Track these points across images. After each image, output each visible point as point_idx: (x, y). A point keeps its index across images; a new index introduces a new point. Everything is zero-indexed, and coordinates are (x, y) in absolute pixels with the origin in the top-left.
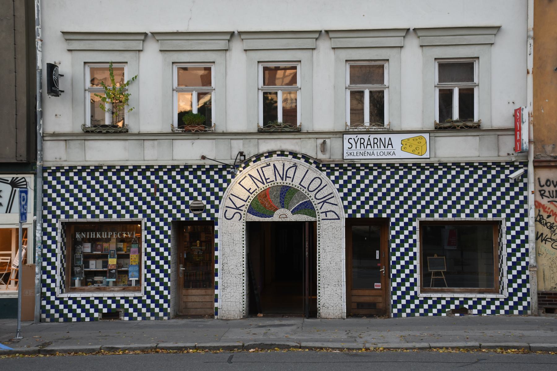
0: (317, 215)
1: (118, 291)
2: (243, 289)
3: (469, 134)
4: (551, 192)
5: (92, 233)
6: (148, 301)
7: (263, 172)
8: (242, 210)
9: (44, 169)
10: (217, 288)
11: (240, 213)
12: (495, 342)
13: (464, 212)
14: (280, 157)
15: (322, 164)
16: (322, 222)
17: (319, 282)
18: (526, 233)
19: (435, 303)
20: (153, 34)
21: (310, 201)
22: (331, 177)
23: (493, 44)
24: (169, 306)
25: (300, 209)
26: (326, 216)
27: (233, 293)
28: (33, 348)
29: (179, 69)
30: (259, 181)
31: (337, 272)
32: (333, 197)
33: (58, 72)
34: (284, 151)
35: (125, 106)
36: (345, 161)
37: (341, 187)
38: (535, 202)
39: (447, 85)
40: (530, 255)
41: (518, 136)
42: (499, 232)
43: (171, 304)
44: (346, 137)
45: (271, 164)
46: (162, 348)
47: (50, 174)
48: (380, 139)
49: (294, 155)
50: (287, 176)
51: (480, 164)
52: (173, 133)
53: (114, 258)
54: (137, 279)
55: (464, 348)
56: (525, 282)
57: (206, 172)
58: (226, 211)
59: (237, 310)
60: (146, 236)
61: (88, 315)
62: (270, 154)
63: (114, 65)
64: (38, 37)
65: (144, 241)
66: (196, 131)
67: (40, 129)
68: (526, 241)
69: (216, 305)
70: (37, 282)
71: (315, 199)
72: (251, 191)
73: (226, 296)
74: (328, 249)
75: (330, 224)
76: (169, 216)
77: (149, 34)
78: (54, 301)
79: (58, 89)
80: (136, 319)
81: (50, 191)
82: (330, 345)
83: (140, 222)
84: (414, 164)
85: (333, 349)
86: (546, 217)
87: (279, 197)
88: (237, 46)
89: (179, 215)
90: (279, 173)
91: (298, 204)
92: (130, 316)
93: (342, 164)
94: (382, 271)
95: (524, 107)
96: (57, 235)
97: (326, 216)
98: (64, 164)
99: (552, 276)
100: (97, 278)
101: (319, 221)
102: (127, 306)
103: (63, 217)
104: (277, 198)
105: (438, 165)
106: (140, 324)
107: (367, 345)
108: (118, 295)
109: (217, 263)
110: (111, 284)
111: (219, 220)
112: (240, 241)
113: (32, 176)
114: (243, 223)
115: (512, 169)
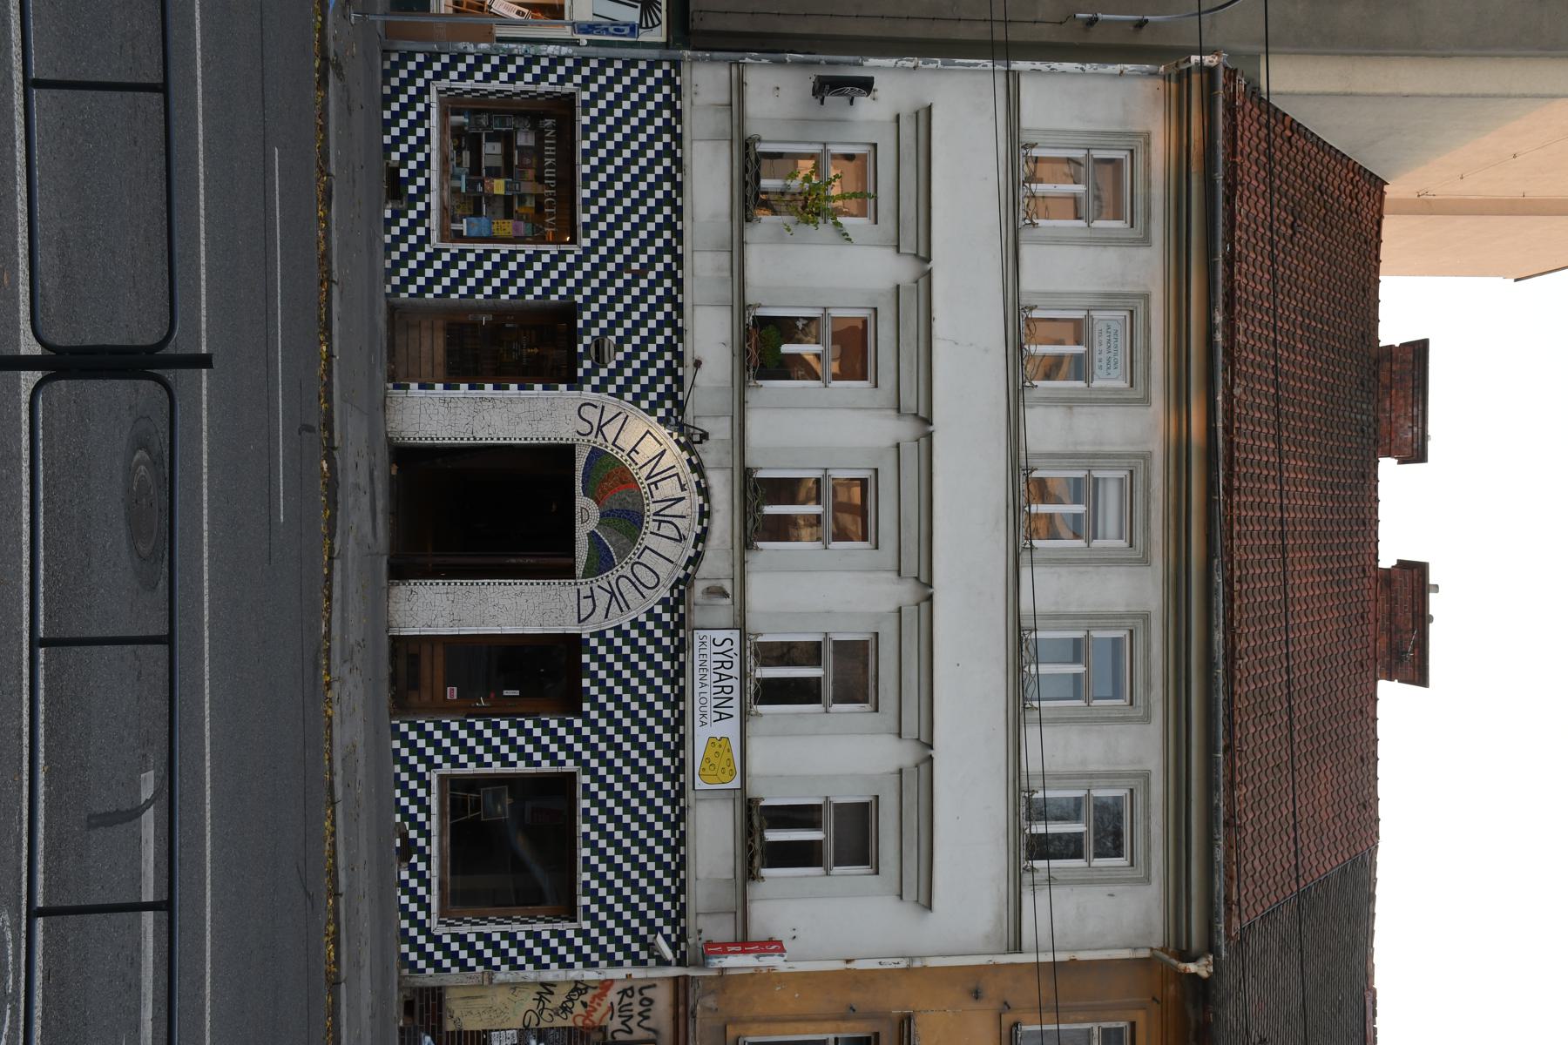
1: (441, 198)
3: (739, 861)
4: (629, 1008)
6: (421, 256)
7: (670, 477)
8: (596, 437)
9: (676, 64)
10: (446, 388)
11: (591, 432)
12: (348, 920)
18: (554, 966)
19: (420, 802)
20: (929, 274)
21: (615, 566)
23: (901, 898)
24: (411, 295)
27: (436, 418)
28: (331, 46)
29: (865, 321)
30: (653, 469)
32: (622, 611)
34: (708, 518)
35: (795, 218)
36: (690, 633)
38: (612, 981)
39: (829, 819)
40: (513, 972)
41: (733, 948)
43: (415, 299)
44: (735, 635)
46: (329, 293)
47: (667, 73)
48: (731, 698)
49: (702, 537)
51: (683, 882)
52: (744, 307)
53: (506, 189)
54: (465, 234)
55: (335, 865)
56: (462, 964)
57: (669, 369)
58: (596, 407)
59: (405, 426)
60: (547, 252)
61: (397, 141)
62: (704, 492)
63: (872, 200)
64: (920, 62)
66: (748, 351)
67: (752, 58)
68: (538, 964)
69: (414, 386)
70: (461, 45)
74: (521, 600)
76: (585, 298)
77: (929, 267)
78: (422, 76)
80: (388, 232)
81: (634, 73)
82: (336, 615)
83: (573, 241)
84: (682, 761)
85: (329, 622)
86: (584, 1000)
88: (905, 430)
89: (587, 315)
92: (394, 221)
94: (480, 702)
95: (785, 958)
96: (551, 84)
98: (686, 100)
99: (474, 1012)
100: (466, 155)
101: (576, 584)
102: (412, 214)
103: (586, 96)
105: (682, 805)
106: (378, 240)
107: (336, 685)
108: (433, 198)
109: (495, 388)
110: (456, 183)
113: (663, 39)
115: (673, 939)
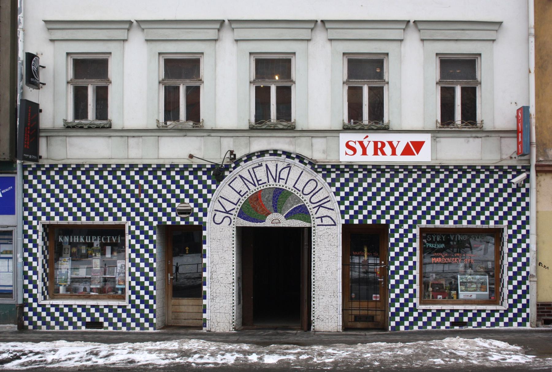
0: (312, 221)
2: (233, 300)
5: (75, 237)
6: (133, 311)
7: (254, 173)
8: (232, 214)
11: (229, 218)
13: (466, 219)
14: (273, 157)
15: (318, 165)
16: (317, 227)
17: (314, 293)
19: (434, 315)
21: (304, 205)
22: (327, 179)
25: (294, 214)
26: (322, 222)
31: (333, 282)
32: (329, 201)
33: (39, 63)
37: (338, 190)
42: (501, 241)
45: (263, 164)
47: (30, 173)
49: (288, 155)
50: (281, 177)
51: (483, 167)
58: (215, 215)
60: (130, 241)
62: (262, 153)
65: (128, 246)
69: (205, 316)
71: (310, 203)
72: (242, 194)
73: (215, 306)
74: (323, 258)
75: (326, 231)
79: (39, 80)
87: (272, 200)
88: (227, 37)
89: (164, 219)
90: (271, 174)
91: (292, 208)
93: (339, 165)
97: (322, 222)
101: (314, 227)
103: (44, 218)
104: (270, 201)
111: (207, 224)
112: (230, 248)
114: (234, 228)
115: (514, 173)
